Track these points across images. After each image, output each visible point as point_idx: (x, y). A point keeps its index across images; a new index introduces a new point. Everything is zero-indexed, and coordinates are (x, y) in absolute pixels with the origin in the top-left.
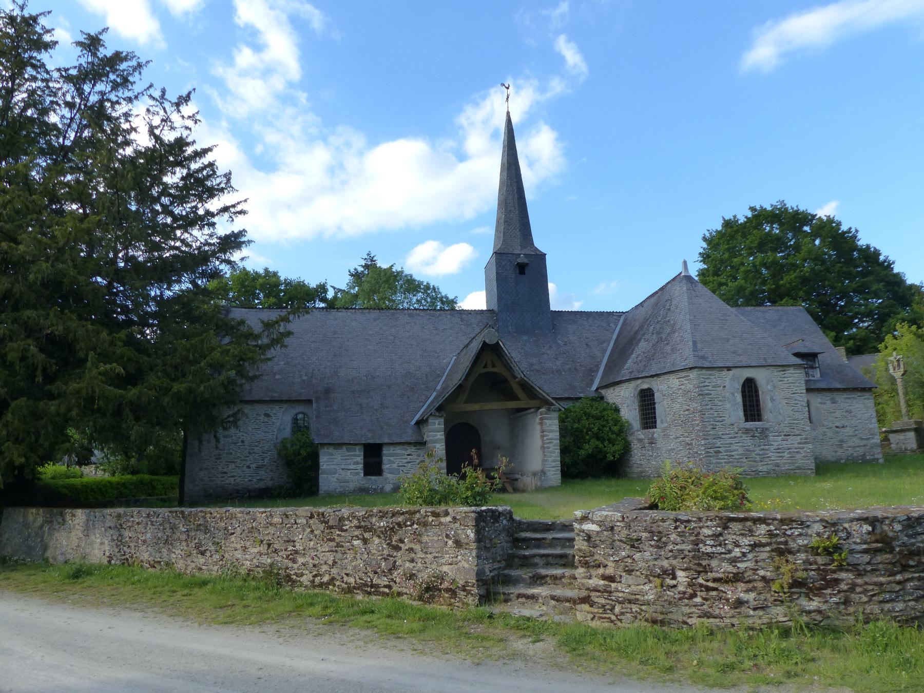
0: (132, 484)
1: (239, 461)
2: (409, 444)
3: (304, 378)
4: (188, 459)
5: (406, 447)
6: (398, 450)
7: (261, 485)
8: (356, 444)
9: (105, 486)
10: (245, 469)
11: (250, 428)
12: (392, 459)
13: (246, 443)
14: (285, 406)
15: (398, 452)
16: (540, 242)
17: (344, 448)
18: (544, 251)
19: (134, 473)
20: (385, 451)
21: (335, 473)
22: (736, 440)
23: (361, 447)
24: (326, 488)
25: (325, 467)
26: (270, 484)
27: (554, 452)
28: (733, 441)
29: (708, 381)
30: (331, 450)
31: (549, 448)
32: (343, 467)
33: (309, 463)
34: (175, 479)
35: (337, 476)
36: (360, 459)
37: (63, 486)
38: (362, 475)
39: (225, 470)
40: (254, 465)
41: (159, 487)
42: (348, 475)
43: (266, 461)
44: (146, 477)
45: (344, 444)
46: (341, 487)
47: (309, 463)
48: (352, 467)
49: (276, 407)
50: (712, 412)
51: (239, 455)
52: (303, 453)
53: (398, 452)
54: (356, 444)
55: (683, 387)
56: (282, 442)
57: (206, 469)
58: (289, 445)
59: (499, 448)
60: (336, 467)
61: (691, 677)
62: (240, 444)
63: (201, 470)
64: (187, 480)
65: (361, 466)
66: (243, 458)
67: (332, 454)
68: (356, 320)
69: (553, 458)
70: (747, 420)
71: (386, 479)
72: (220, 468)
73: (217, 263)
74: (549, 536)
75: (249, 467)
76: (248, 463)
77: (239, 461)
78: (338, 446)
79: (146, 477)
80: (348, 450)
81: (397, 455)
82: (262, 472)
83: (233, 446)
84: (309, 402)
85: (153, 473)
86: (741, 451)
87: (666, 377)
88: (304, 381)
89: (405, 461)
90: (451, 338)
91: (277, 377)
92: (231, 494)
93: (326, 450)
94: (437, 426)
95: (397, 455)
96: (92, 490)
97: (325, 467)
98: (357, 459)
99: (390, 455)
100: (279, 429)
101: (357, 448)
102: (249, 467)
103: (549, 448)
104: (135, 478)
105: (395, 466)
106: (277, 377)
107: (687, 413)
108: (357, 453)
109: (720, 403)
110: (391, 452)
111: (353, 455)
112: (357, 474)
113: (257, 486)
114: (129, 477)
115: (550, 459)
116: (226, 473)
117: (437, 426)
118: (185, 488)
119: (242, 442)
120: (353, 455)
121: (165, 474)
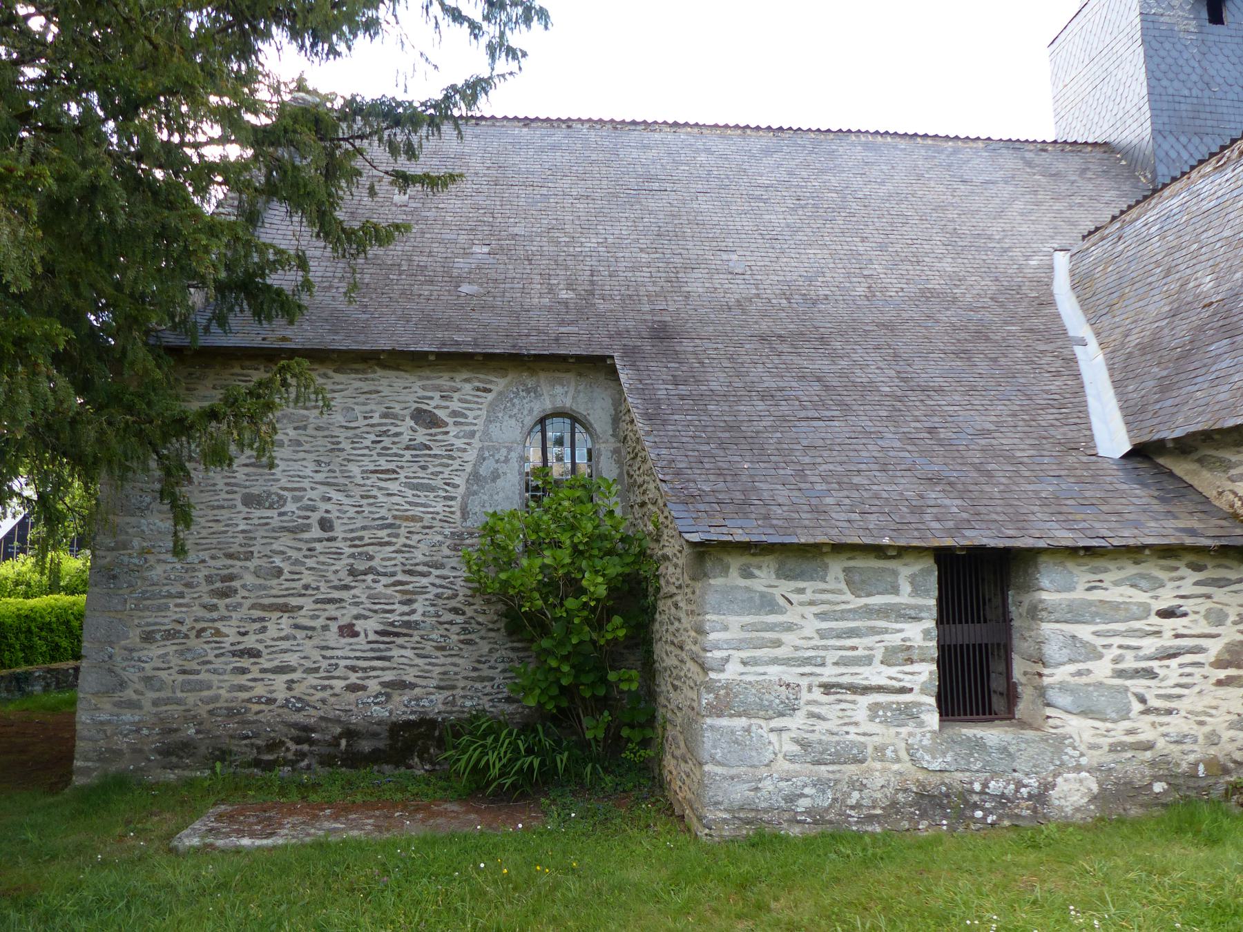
1: (308, 603)
2: (1168, 552)
3: (564, 295)
5: (1154, 569)
6: (1116, 587)
7: (400, 708)
8: (902, 552)
10: (332, 637)
11: (355, 469)
12: (1084, 632)
13: (339, 531)
14: (499, 384)
15: (1115, 594)
17: (836, 567)
20: (1055, 589)
21: (790, 709)
23: (928, 572)
24: (739, 793)
25: (732, 671)
26: (435, 704)
30: (765, 579)
32: (829, 673)
33: (617, 629)
35: (796, 722)
36: (920, 632)
38: (932, 719)
39: (250, 642)
40: (372, 624)
42: (857, 721)
43: (419, 606)
45: (839, 549)
46: (821, 784)
47: (617, 629)
48: (877, 674)
49: (465, 385)
51: (308, 578)
52: (596, 586)
53: (1115, 594)
54: (902, 552)
56: (490, 530)
57: (170, 635)
58: (517, 546)
60: (790, 674)
62: (316, 532)
63: (148, 638)
65: (926, 672)
66: (325, 592)
67: (768, 604)
68: (708, 151)
71: (1061, 742)
72: (230, 631)
75: (348, 631)
77: (308, 603)
78: (800, 556)
80: (856, 586)
81: (1112, 611)
82: (401, 653)
83: (285, 541)
84: (596, 366)
88: (565, 303)
89: (1150, 645)
90: (1019, 205)
91: (465, 288)
92: (273, 746)
93: (735, 579)
95: (1112, 611)
96: (46, 627)
97: (732, 671)
98: (905, 629)
99: (1076, 614)
100: (475, 477)
101: (905, 571)
102: (348, 631)
105: (1102, 670)
106: (465, 288)
108: (905, 596)
110: (1079, 594)
111: (884, 612)
112: (908, 713)
113: (379, 712)
116: (253, 654)
119: (325, 524)
120: (884, 612)
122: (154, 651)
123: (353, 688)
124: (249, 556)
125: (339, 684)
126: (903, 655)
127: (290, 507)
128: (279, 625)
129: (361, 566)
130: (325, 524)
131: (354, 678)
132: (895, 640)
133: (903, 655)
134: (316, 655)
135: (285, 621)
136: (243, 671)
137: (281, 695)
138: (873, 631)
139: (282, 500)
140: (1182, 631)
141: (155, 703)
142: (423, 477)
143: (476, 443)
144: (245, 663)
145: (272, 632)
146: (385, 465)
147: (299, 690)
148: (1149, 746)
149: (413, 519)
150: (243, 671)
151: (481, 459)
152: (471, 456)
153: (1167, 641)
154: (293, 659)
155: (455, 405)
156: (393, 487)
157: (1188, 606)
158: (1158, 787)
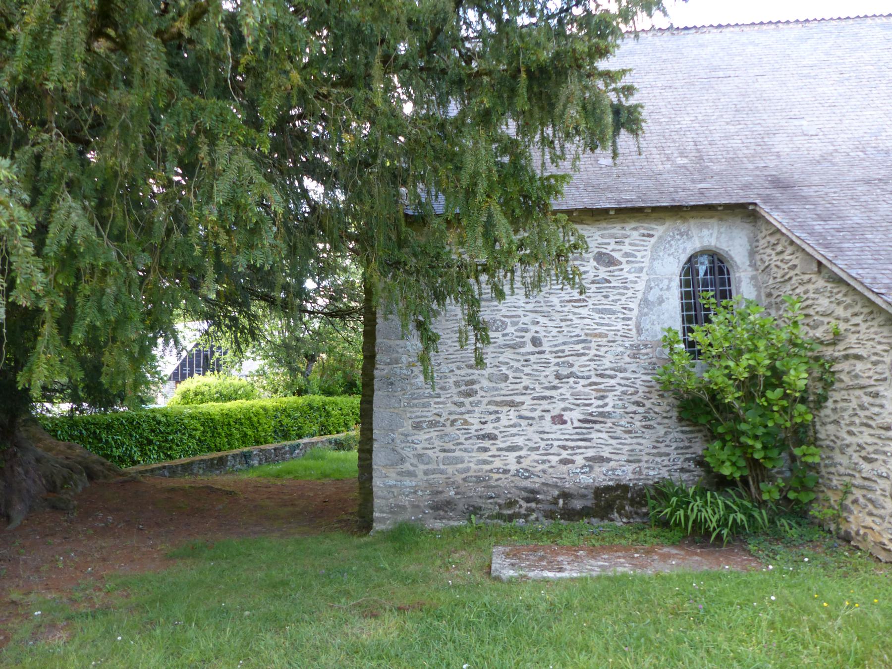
0: (296, 409)
1: (527, 399)
4: (379, 396)
7: (600, 476)
9: (257, 414)
10: (547, 424)
13: (546, 347)
14: (659, 230)
19: (300, 392)
26: (627, 474)
34: (355, 400)
37: (191, 417)
39: (489, 428)
40: (575, 415)
41: (336, 412)
44: (318, 399)
51: (526, 381)
57: (433, 424)
61: (859, 585)
62: (529, 348)
63: (417, 426)
64: (379, 457)
66: (539, 391)
72: (474, 421)
76: (556, 410)
79: (318, 399)
83: (508, 354)
85: (328, 393)
92: (511, 504)
96: (238, 421)
102: (559, 420)
104: (300, 400)
114: (292, 399)
116: (492, 437)
118: (377, 482)
121: (344, 392)
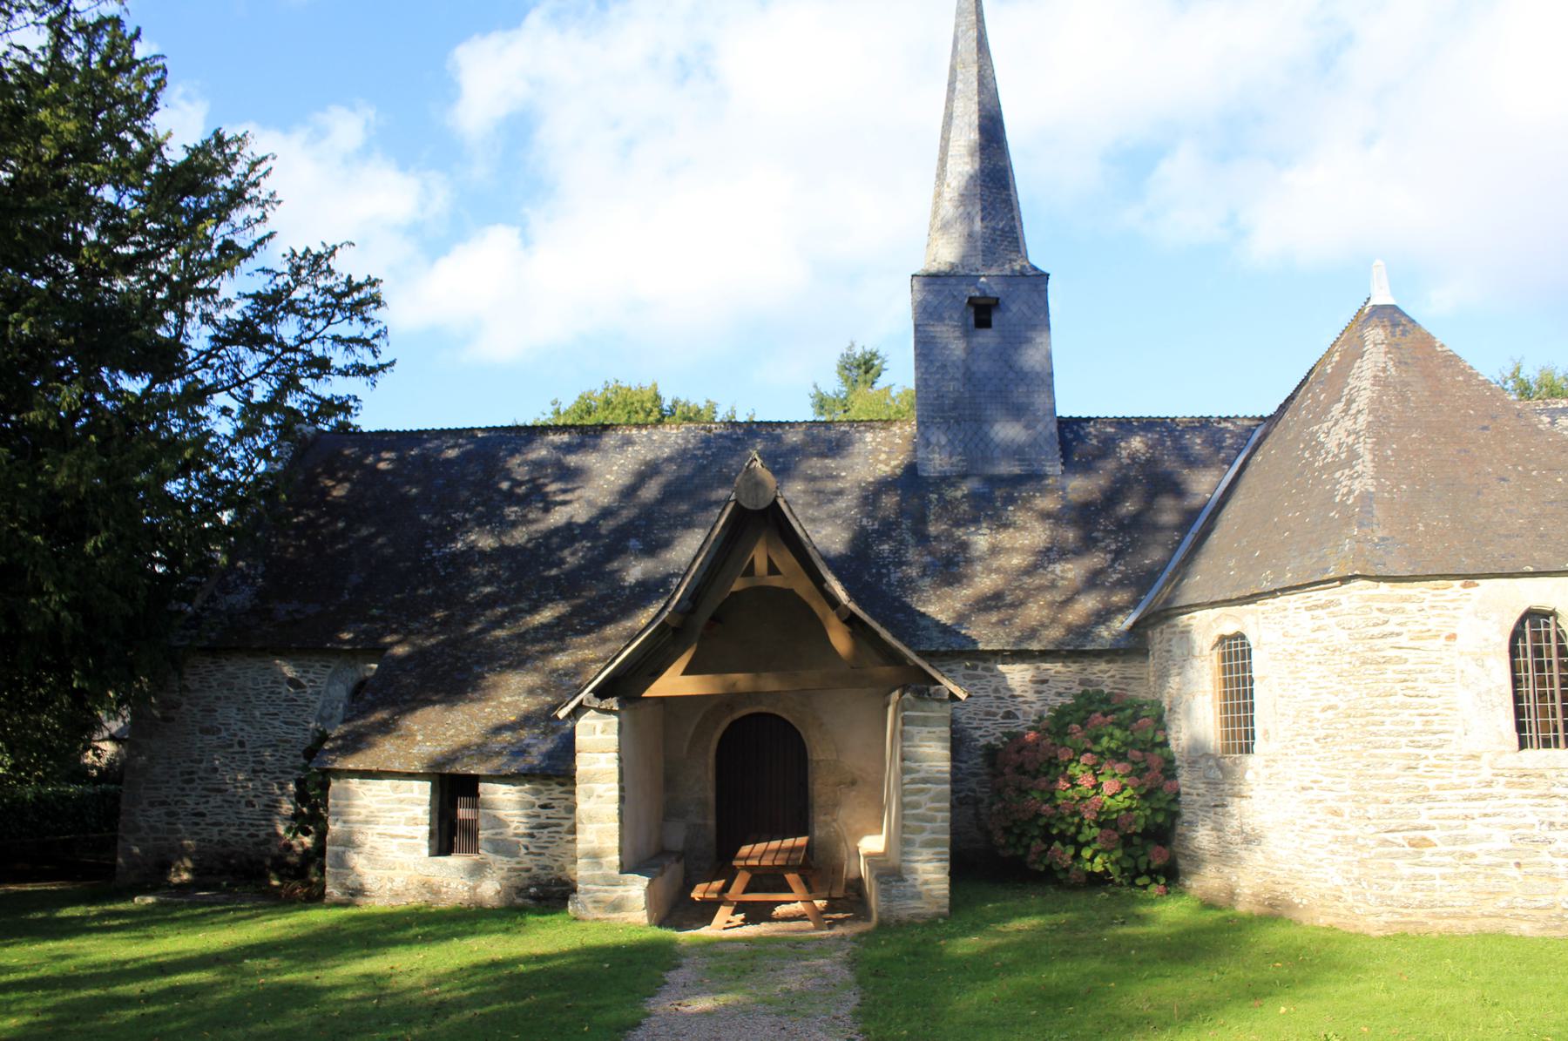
11: (257, 713)
13: (248, 748)
16: (1038, 251)
18: (1043, 267)
22: (1490, 806)
27: (932, 820)
28: (1475, 808)
29: (1395, 619)
31: (916, 806)
39: (201, 808)
48: (401, 830)
50: (1405, 715)
55: (1320, 635)
57: (163, 803)
59: (853, 783)
62: (237, 748)
63: (152, 804)
69: (926, 836)
70: (1523, 745)
72: (190, 802)
73: (214, 469)
74: (121, 990)
86: (1501, 840)
87: (1281, 601)
94: (598, 736)
96: (1012, 210)
103: (916, 806)
107: (1330, 714)
109: (1434, 690)
115: (918, 838)
116: (202, 815)
117: (598, 736)
119: (242, 744)
122: (155, 812)
123: (251, 835)
124: (201, 761)
125: (244, 833)
126: (414, 821)
127: (224, 734)
128: (216, 800)
129: (259, 768)
130: (242, 744)
131: (252, 830)
132: (410, 814)
133: (414, 821)
134: (233, 816)
135: (219, 798)
136: (197, 824)
137: (216, 838)
138: (400, 810)
139: (219, 730)
140: (1489, 811)
141: (155, 839)
142: (293, 718)
143: (321, 698)
144: (197, 820)
145: (212, 803)
146: (272, 710)
147: (225, 836)
148: (528, 870)
149: (286, 741)
150: (197, 824)
151: (324, 707)
152: (318, 705)
153: (543, 820)
154: (222, 819)
155: (311, 676)
156: (277, 723)
157: (555, 803)
158: (532, 890)
